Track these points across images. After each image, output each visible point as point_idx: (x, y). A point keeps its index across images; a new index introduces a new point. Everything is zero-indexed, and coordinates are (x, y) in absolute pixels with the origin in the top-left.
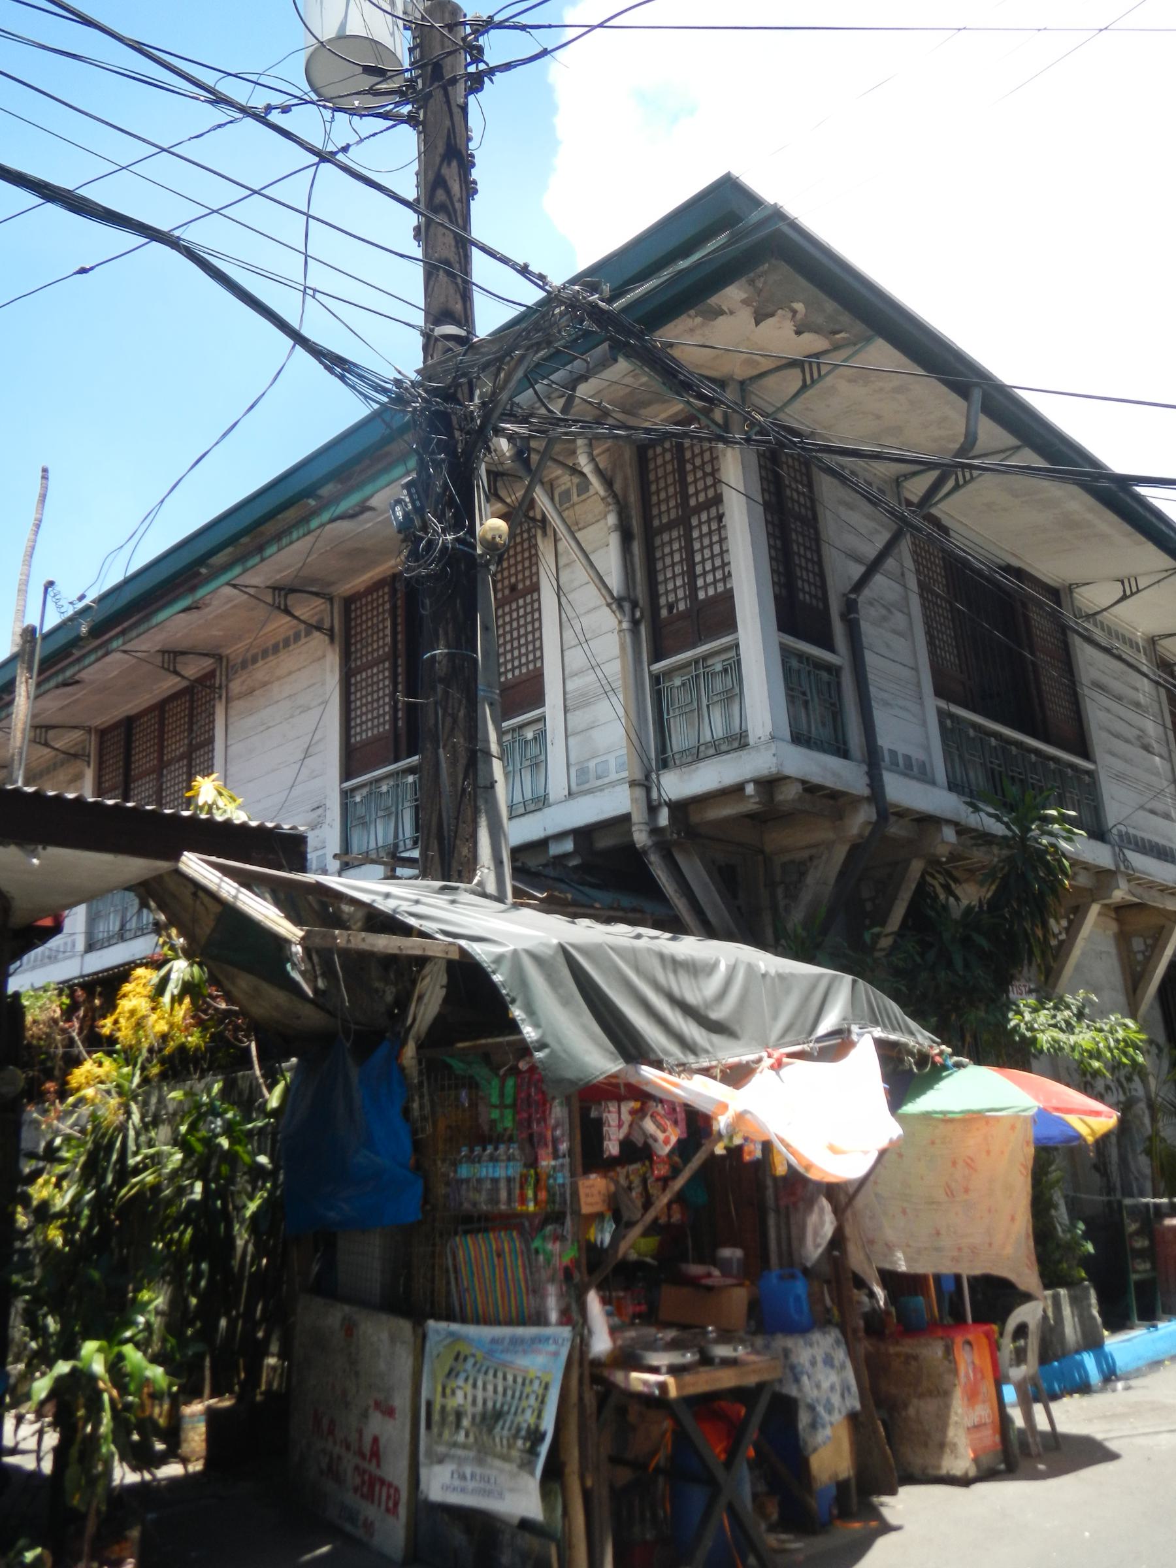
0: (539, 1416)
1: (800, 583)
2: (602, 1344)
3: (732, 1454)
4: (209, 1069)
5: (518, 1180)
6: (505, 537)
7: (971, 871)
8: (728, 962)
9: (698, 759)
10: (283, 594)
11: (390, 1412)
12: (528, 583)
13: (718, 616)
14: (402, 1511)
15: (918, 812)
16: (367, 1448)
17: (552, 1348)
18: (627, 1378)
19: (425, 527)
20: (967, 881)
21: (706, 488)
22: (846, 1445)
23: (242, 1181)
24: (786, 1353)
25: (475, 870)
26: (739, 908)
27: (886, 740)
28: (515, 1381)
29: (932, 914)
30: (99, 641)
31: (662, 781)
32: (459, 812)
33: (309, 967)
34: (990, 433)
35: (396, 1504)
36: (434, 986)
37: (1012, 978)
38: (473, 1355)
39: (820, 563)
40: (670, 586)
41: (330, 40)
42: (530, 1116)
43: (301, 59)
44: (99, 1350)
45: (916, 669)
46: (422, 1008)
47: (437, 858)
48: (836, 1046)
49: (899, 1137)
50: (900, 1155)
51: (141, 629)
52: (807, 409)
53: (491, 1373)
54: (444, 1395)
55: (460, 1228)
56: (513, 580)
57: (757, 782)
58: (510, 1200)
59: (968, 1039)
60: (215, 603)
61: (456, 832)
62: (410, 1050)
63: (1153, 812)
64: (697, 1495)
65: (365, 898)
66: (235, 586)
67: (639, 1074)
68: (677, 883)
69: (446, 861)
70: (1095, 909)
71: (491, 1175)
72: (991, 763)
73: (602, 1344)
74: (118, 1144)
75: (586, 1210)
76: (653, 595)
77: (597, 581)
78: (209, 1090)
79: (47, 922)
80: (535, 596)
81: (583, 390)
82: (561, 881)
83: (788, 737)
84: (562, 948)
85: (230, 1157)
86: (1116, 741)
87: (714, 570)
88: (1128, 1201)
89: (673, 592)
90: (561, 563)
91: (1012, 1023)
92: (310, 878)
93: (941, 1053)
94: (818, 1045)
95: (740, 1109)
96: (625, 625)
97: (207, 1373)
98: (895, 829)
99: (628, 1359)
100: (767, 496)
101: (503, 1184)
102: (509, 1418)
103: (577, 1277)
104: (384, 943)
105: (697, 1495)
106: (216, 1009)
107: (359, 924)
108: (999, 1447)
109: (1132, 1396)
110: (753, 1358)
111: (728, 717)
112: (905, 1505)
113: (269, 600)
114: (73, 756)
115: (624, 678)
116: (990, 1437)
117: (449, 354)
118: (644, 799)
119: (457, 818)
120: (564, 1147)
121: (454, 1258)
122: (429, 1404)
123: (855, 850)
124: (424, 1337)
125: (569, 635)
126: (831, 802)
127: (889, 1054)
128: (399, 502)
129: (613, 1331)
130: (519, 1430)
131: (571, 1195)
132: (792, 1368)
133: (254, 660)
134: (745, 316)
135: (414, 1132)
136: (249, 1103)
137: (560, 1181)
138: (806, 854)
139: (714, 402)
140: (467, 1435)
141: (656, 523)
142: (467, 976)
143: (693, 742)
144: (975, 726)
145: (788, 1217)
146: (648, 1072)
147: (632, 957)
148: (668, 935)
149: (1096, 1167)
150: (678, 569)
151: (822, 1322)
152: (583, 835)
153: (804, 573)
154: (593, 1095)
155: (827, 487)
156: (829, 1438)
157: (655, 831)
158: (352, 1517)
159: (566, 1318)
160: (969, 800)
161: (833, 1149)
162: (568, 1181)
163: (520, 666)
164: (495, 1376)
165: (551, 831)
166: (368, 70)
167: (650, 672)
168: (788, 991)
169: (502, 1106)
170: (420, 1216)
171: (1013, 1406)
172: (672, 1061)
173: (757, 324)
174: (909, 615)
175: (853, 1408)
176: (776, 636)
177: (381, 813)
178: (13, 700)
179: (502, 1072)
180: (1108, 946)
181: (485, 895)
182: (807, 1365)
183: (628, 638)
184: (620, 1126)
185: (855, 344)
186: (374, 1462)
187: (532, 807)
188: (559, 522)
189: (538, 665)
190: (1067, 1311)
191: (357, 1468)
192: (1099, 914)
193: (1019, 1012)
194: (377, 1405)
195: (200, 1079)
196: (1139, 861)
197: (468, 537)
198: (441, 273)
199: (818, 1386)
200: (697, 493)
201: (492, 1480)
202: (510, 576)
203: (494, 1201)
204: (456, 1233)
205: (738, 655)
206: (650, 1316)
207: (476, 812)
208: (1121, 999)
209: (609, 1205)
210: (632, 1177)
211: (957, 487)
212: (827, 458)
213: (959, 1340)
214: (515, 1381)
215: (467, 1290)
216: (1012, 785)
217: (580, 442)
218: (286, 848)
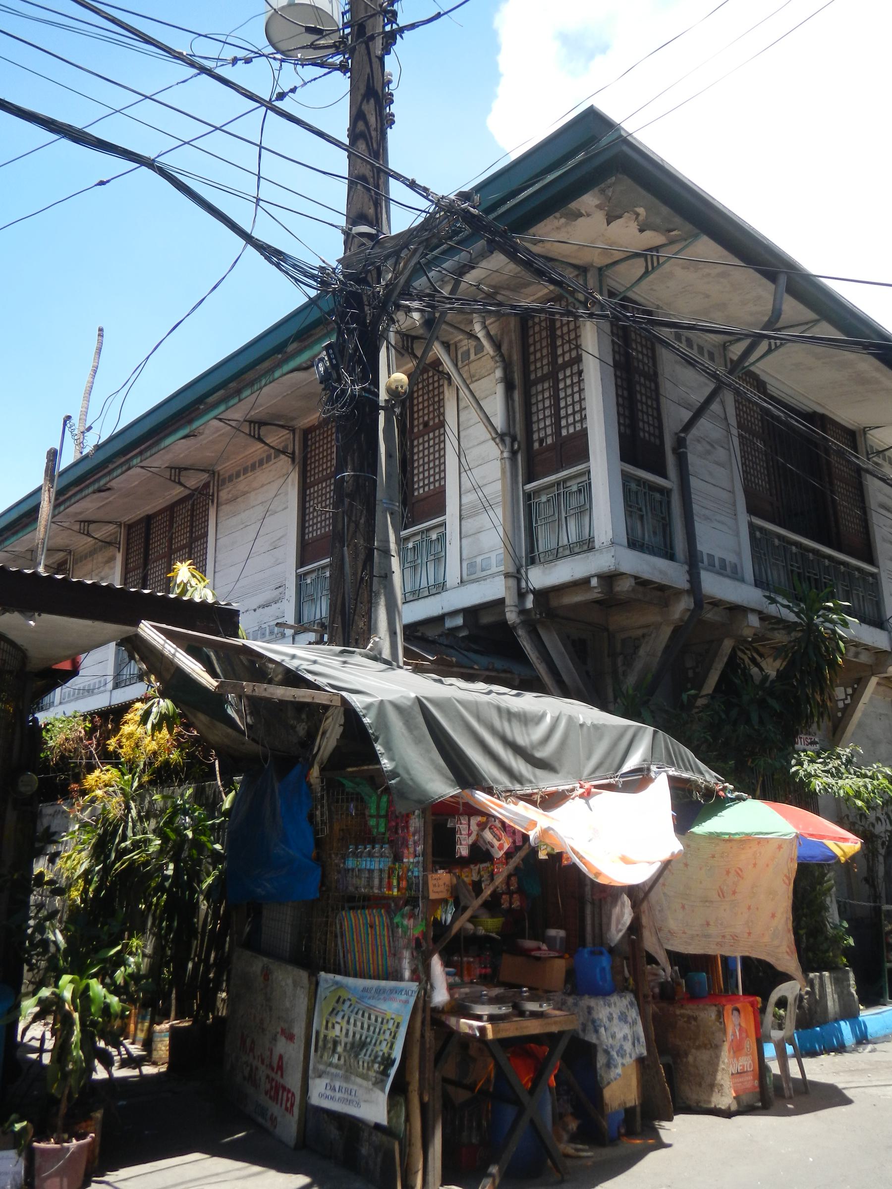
0: (391, 1048)
1: (641, 424)
3: (536, 1082)
5: (387, 872)
6: (406, 387)
8: (554, 713)
9: (557, 558)
10: (257, 426)
11: (291, 1037)
13: (575, 449)
14: (296, 1110)
15: (728, 603)
17: (404, 997)
18: (458, 1022)
19: (339, 379)
21: (570, 350)
22: (634, 1082)
23: (206, 861)
24: (590, 1010)
25: (369, 639)
26: (587, 673)
27: (704, 546)
28: (376, 1021)
30: (123, 459)
32: (358, 595)
34: (792, 309)
35: (292, 1105)
36: (335, 724)
38: (350, 1000)
39: (658, 409)
40: (542, 425)
41: (283, 8)
42: (397, 824)
43: (262, 21)
44: (71, 982)
45: (732, 492)
46: (325, 740)
47: (340, 630)
48: (638, 781)
49: (680, 851)
50: (686, 865)
51: (154, 450)
52: (652, 289)
53: (361, 1013)
55: (346, 905)
56: (426, 418)
57: (600, 576)
58: (380, 887)
60: (207, 432)
61: (355, 611)
62: (315, 772)
64: (510, 1112)
65: (277, 658)
66: (220, 420)
67: (474, 797)
68: (539, 652)
69: (346, 628)
70: (874, 680)
71: (368, 867)
72: (792, 565)
73: (441, 996)
74: (120, 831)
75: (433, 896)
77: (485, 421)
78: (182, 795)
79: (66, 666)
80: (442, 431)
81: (471, 278)
82: (452, 647)
83: (626, 543)
84: (417, 698)
87: (574, 413)
89: (544, 430)
90: (461, 407)
91: (794, 769)
93: (724, 789)
94: (621, 780)
95: (545, 826)
96: (506, 455)
97: (174, 1002)
98: (710, 615)
99: (461, 1009)
100: (617, 357)
101: (376, 874)
102: (370, 1048)
104: (281, 692)
105: (510, 1112)
108: (758, 1090)
109: (875, 1056)
110: (557, 1013)
111: (580, 526)
112: (679, 1129)
114: (108, 543)
115: (504, 496)
116: (750, 1082)
117: (363, 248)
118: (516, 587)
119: (356, 600)
120: (420, 849)
121: (341, 927)
122: (318, 1033)
123: (677, 631)
124: (317, 984)
126: (659, 593)
128: (322, 360)
129: (451, 987)
130: (376, 1057)
131: (423, 884)
132: (593, 1021)
133: (238, 475)
134: (599, 217)
135: (316, 833)
136: (212, 805)
137: (416, 874)
138: (640, 632)
139: (572, 286)
140: (339, 1059)
141: (533, 377)
142: (351, 715)
146: (481, 796)
147: (475, 709)
149: (866, 880)
150: (547, 413)
151: (620, 988)
152: (471, 613)
153: (645, 417)
154: (442, 817)
156: (619, 1075)
157: (523, 612)
158: (263, 1111)
159: (415, 977)
160: (767, 594)
161: (625, 860)
162: (421, 874)
163: (429, 483)
164: (363, 1016)
165: (447, 610)
166: (309, 30)
167: (523, 490)
168: (600, 738)
169: (378, 816)
170: (318, 895)
171: (772, 1059)
172: (500, 788)
173: (608, 224)
175: (642, 1054)
176: (618, 465)
178: (392, 703)
181: (375, 658)
182: (605, 1020)
184: (469, 835)
185: (686, 240)
186: (279, 1073)
187: (434, 591)
189: (442, 483)
190: (829, 989)
191: (268, 1077)
192: (878, 684)
193: (801, 764)
195: (179, 786)
197: (372, 387)
198: (359, 187)
199: (613, 1036)
200: (564, 354)
201: (353, 1093)
203: (370, 885)
204: (343, 909)
205: (589, 479)
206: (488, 980)
209: (451, 893)
210: (482, 873)
211: (770, 351)
213: (729, 1008)
214: (376, 1021)
216: (808, 584)
218: (223, 619)
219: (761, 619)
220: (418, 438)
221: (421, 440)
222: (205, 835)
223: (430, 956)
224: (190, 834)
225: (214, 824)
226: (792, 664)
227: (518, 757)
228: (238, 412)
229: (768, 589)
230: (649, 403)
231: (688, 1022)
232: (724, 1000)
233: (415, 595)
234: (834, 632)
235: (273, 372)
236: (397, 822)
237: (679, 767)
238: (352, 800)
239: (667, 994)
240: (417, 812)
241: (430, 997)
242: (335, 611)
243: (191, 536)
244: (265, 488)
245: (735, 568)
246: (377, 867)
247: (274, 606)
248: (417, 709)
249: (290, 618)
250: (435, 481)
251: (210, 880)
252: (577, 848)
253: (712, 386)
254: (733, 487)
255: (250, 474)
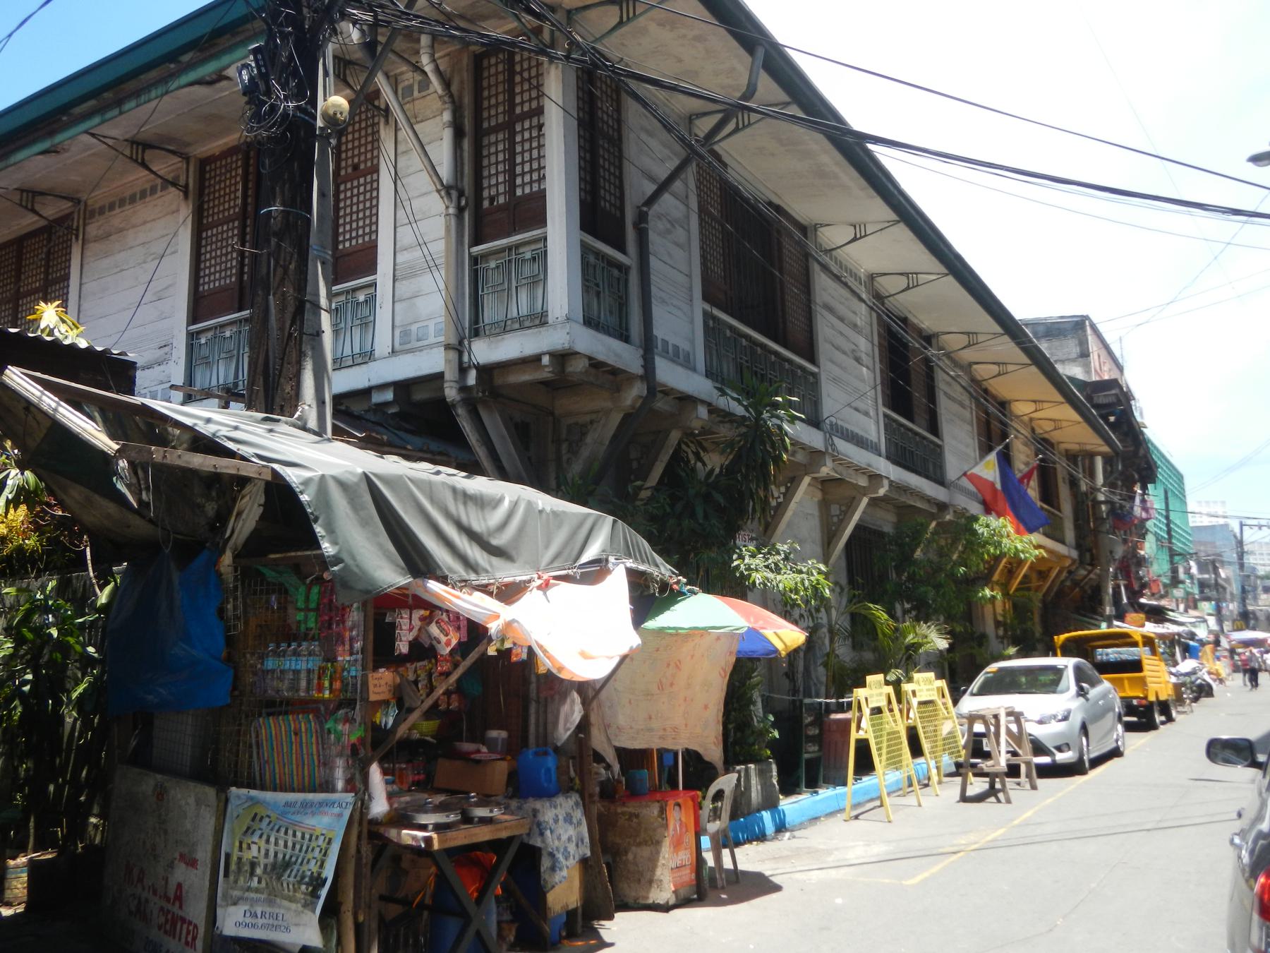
0: (322, 866)
1: (602, 192)
2: (380, 807)
3: (482, 892)
4: (45, 570)
6: (346, 114)
7: (717, 444)
9: (505, 330)
10: (140, 149)
11: (192, 863)
12: (369, 164)
13: (530, 212)
14: (199, 944)
15: (679, 392)
16: (171, 894)
17: (337, 810)
18: (399, 834)
19: (268, 92)
20: (713, 451)
21: (530, 100)
22: (576, 883)
23: (73, 669)
24: (535, 812)
25: (296, 406)
26: (529, 458)
27: (659, 332)
28: (303, 837)
29: (683, 474)
31: (473, 347)
33: (134, 481)
34: (768, 89)
35: (194, 939)
37: (739, 528)
40: (493, 181)
42: (331, 618)
45: (689, 276)
47: (261, 394)
48: (595, 572)
52: (623, 44)
53: (283, 830)
54: (241, 848)
56: (356, 160)
57: (555, 355)
58: (308, 689)
59: (701, 573)
61: (281, 372)
62: (227, 559)
63: (857, 409)
64: (453, 925)
65: (188, 421)
66: (93, 135)
69: (270, 394)
70: (807, 480)
73: (380, 807)
75: (373, 698)
76: (478, 187)
78: (43, 588)
80: (375, 177)
84: (365, 475)
85: (61, 646)
86: (837, 352)
87: (531, 171)
88: (807, 701)
89: (496, 187)
90: (399, 151)
91: (735, 563)
92: (137, 400)
93: (678, 582)
95: (508, 619)
96: (451, 211)
98: (661, 404)
99: (401, 819)
101: (303, 675)
102: (296, 867)
103: (362, 753)
104: (199, 461)
105: (453, 925)
106: (53, 516)
107: (185, 446)
110: (506, 817)
111: (532, 299)
113: (128, 152)
115: (447, 257)
116: (688, 875)
119: (282, 359)
120: (358, 645)
121: (257, 736)
122: (228, 856)
123: (627, 417)
124: (227, 800)
125: (401, 213)
126: (611, 377)
127: (638, 582)
128: (246, 66)
129: (390, 796)
130: (303, 877)
132: (539, 824)
133: (112, 207)
136: (83, 600)
137: (353, 673)
138: (588, 418)
140: (259, 882)
141: (485, 125)
142: (279, 493)
143: (502, 317)
144: (732, 328)
145: (546, 706)
146: (433, 585)
147: (429, 489)
148: (464, 474)
149: (787, 675)
150: (501, 167)
151: (566, 788)
152: (403, 387)
154: (385, 606)
155: (632, 111)
157: (464, 389)
159: (350, 786)
161: (584, 655)
162: (359, 674)
163: (357, 236)
164: (286, 833)
165: (374, 382)
168: (559, 526)
169: (307, 609)
172: (456, 577)
174: (688, 231)
176: (578, 234)
177: (223, 355)
178: (334, 478)
179: (308, 581)
180: (812, 509)
181: (304, 428)
182: (551, 821)
183: (453, 222)
184: (411, 630)
186: (177, 904)
187: (360, 361)
188: (398, 111)
189: (374, 237)
190: (754, 781)
191: (162, 909)
193: (741, 557)
194: (182, 857)
195: (36, 578)
196: (843, 446)
199: (559, 838)
200: (522, 103)
202: (353, 157)
203: (294, 687)
204: (260, 715)
206: (426, 785)
207: (301, 356)
208: (819, 550)
212: (633, 84)
213: (671, 802)
214: (303, 837)
215: (267, 762)
217: (425, 40)
218: (117, 372)
219: (710, 412)
220: (345, 182)
221: (349, 185)
222: (72, 636)
223: (370, 764)
224: (54, 632)
225: (84, 623)
226: (738, 457)
227: (474, 544)
228: (120, 126)
229: (723, 383)
230: (612, 170)
231: (630, 819)
232: (658, 796)
233: (339, 364)
234: (780, 428)
235: (167, 83)
236: (331, 613)
237: (636, 559)
238: (274, 592)
239: (608, 792)
240: (355, 605)
241: (368, 808)
242: (255, 371)
243: (46, 278)
244: (148, 225)
245: (687, 355)
246: (304, 666)
247: (157, 369)
248: (364, 486)
249: (179, 379)
250: (364, 234)
251: (80, 689)
252: (541, 642)
253: (683, 154)
254: (691, 271)
255: (127, 207)
